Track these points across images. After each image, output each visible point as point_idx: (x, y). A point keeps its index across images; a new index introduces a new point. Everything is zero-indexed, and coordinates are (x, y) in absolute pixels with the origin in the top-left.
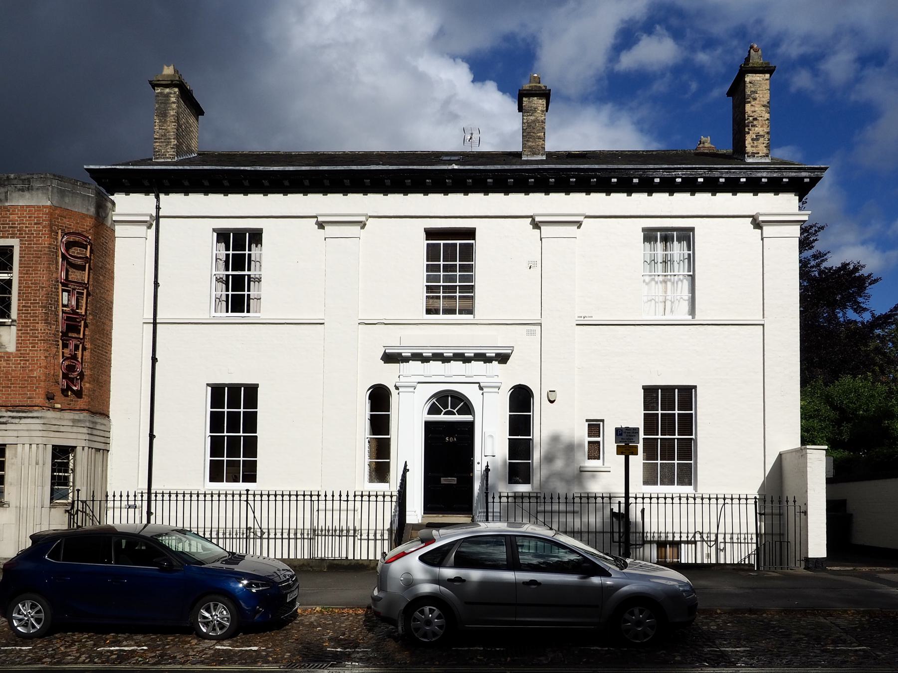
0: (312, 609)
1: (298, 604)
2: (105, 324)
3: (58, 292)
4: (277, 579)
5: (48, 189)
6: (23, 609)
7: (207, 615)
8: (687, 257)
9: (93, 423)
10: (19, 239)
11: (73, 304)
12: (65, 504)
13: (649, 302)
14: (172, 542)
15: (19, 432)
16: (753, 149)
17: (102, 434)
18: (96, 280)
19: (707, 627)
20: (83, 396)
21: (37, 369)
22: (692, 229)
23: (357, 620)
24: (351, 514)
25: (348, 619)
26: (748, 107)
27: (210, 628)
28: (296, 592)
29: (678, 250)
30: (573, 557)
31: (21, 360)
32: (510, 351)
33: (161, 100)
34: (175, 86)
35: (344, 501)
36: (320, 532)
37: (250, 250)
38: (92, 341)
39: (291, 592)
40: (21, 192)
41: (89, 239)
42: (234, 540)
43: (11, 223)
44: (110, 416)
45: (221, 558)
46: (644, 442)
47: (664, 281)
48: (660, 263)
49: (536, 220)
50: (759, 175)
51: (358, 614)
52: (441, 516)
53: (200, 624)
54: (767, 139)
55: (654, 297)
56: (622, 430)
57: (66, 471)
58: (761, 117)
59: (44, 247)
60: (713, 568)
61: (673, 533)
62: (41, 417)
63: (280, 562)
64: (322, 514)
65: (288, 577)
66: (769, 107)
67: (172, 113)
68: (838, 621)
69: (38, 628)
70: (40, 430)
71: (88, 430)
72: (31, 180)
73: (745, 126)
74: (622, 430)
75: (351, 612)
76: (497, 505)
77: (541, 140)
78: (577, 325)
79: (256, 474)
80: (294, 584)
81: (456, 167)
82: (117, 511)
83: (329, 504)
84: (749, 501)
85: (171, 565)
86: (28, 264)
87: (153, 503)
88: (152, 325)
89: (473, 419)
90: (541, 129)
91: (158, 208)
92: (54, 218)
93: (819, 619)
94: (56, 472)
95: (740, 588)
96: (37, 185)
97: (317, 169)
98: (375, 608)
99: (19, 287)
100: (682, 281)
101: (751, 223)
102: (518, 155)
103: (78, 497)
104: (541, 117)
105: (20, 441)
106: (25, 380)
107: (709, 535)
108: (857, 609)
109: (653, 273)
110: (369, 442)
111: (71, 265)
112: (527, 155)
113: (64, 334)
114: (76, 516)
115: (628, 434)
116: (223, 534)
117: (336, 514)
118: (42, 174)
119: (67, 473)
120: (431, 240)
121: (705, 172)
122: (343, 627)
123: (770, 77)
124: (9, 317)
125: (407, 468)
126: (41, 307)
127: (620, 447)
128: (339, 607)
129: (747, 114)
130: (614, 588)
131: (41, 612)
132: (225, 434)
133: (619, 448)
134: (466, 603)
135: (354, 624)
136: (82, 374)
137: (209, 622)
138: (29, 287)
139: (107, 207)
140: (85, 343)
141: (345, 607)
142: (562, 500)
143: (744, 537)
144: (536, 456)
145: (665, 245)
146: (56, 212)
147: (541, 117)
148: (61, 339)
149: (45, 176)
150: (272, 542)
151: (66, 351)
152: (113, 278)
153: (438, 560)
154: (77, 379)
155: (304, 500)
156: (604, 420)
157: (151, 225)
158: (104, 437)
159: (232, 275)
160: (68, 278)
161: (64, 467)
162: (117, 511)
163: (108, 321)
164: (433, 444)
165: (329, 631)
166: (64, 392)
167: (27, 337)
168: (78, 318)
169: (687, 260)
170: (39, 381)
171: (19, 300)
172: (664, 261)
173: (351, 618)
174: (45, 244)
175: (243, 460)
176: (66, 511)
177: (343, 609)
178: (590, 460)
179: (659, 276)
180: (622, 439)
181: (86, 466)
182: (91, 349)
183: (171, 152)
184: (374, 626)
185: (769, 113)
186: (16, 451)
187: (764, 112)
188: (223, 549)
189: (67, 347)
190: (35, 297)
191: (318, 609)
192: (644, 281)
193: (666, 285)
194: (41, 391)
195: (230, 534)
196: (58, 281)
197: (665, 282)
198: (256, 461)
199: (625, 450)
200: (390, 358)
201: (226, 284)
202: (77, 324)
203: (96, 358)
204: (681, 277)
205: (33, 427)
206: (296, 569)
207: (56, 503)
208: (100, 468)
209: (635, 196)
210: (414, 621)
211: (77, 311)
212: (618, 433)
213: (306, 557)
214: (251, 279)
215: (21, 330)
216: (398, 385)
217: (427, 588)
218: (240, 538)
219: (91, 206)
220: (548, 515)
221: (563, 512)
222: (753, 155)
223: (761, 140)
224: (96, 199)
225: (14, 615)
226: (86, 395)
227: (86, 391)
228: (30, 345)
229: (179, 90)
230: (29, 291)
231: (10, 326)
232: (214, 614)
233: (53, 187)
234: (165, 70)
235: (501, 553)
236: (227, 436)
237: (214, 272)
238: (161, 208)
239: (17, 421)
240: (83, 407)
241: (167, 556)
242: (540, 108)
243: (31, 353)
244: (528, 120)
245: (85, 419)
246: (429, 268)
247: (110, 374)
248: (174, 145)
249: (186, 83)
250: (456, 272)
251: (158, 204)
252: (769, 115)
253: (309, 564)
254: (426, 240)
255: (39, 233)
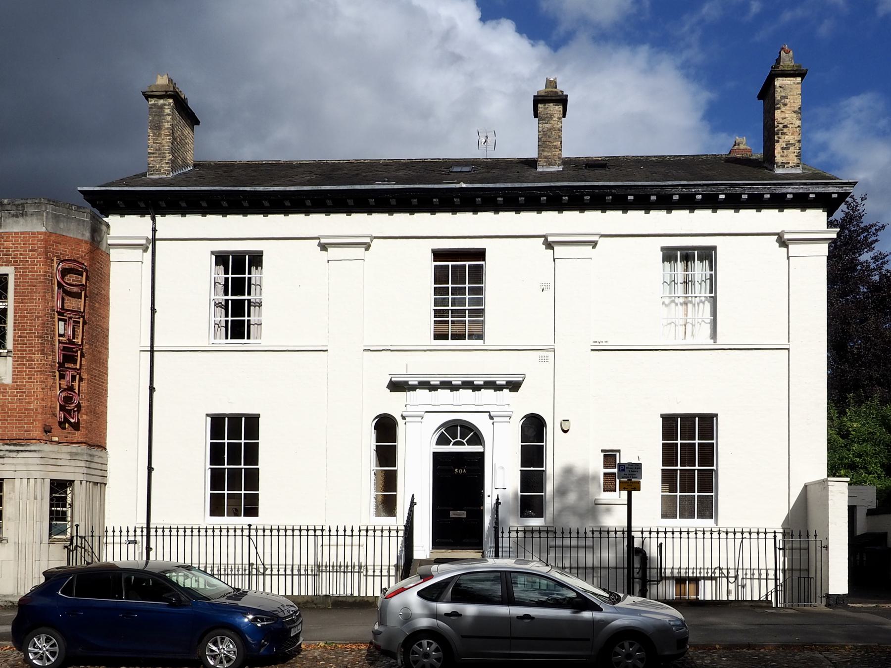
0: (315, 645)
1: (301, 639)
2: (101, 352)
3: (54, 321)
4: (281, 615)
5: (42, 215)
6: (38, 643)
7: (214, 648)
8: (709, 277)
9: (91, 455)
10: (13, 267)
11: (69, 333)
12: (64, 540)
13: (669, 326)
14: (180, 578)
15: (17, 466)
16: (783, 158)
17: (99, 467)
18: (92, 308)
19: (701, 661)
20: (80, 429)
21: (34, 401)
22: (714, 248)
23: (360, 655)
24: (356, 549)
25: (351, 654)
26: (778, 114)
27: (217, 660)
28: (299, 627)
29: (699, 269)
30: (574, 595)
31: (17, 392)
32: (521, 379)
33: (153, 112)
34: (170, 97)
35: (349, 536)
36: (324, 568)
37: (250, 273)
38: (89, 371)
39: (295, 627)
40: (15, 218)
41: (85, 265)
42: (230, 576)
43: (5, 250)
44: (107, 448)
45: (227, 594)
46: (662, 473)
47: (685, 304)
48: (681, 283)
49: (549, 240)
50: (784, 191)
51: (361, 649)
52: (450, 551)
53: (208, 657)
54: (798, 148)
55: (674, 321)
56: (624, 466)
57: (64, 506)
58: (792, 124)
59: (39, 275)
60: (730, 605)
61: (728, 569)
62: (39, 451)
63: (284, 598)
64: (326, 549)
65: (291, 613)
66: (800, 113)
67: (167, 125)
68: (833, 656)
69: (53, 661)
70: (38, 464)
71: (86, 463)
72: (25, 205)
73: (774, 134)
74: (624, 466)
75: (354, 647)
76: (506, 540)
77: (558, 150)
78: (592, 350)
79: (258, 508)
80: (297, 619)
81: (464, 185)
82: (117, 547)
83: (334, 539)
84: (768, 535)
85: (179, 600)
86: (23, 292)
87: (152, 539)
88: (149, 353)
89: (483, 450)
90: (557, 137)
91: (154, 230)
92: (50, 245)
93: (815, 654)
94: (54, 507)
95: (748, 624)
96: (31, 210)
97: (319, 189)
98: (376, 642)
99: (15, 316)
100: (703, 303)
101: (776, 241)
102: (531, 163)
103: (77, 533)
104: (558, 124)
105: (18, 475)
106: (22, 413)
107: (695, 571)
108: (855, 644)
109: (673, 295)
110: (375, 474)
111: (67, 293)
112: (543, 166)
113: (61, 365)
114: (75, 552)
115: (630, 470)
116: (218, 571)
117: (341, 549)
118: (36, 199)
119: (65, 507)
120: (440, 261)
121: (726, 188)
122: (345, 661)
123: (802, 81)
124: (4, 348)
125: (415, 501)
126: (38, 337)
127: (623, 483)
128: (342, 642)
129: (776, 121)
130: (604, 623)
131: (56, 646)
132: (226, 466)
133: (621, 484)
134: (463, 637)
135: (356, 658)
136: (79, 406)
137: (216, 655)
138: (25, 317)
139: (102, 230)
140: (82, 374)
141: (348, 642)
142: (574, 535)
143: (692, 571)
144: (549, 488)
145: (685, 265)
146: (52, 238)
147: (558, 124)
148: (58, 370)
149: (40, 202)
150: (275, 578)
151: (63, 382)
152: (108, 304)
153: (435, 595)
154: (74, 411)
155: (308, 535)
156: (620, 450)
157: (148, 248)
158: (101, 470)
159: (231, 300)
160: (64, 306)
161: (61, 502)
162: (117, 547)
163: (103, 349)
164: (442, 476)
165: (331, 665)
166: (61, 424)
167: (23, 368)
168: (74, 348)
169: (708, 280)
170: (36, 413)
171: (15, 330)
172: (684, 282)
173: (353, 653)
174: (40, 272)
175: (244, 494)
176: (65, 547)
177: (346, 644)
178: (606, 493)
179: (679, 297)
180: (625, 474)
181: (84, 503)
182: (88, 380)
183: (166, 167)
184: (376, 660)
185: (800, 120)
186: (14, 486)
187: (795, 119)
188: (224, 583)
189: (64, 378)
190: (31, 326)
191: (322, 644)
192: (663, 303)
193: (687, 307)
194: (39, 424)
195: (225, 571)
196: (54, 310)
197: (686, 304)
198: (258, 494)
199: (628, 485)
200: (396, 386)
201: (225, 309)
202: (74, 354)
203: (93, 388)
204: (703, 299)
205: (30, 461)
206: (300, 606)
207: (55, 538)
208: (98, 502)
209: (653, 213)
210: (413, 654)
211: (74, 340)
212: (621, 469)
213: (310, 594)
214: (252, 304)
215: (17, 361)
216: (404, 414)
217: (424, 623)
218: (235, 575)
219: (86, 231)
220: (559, 550)
221: (574, 547)
222: (783, 165)
223: (792, 149)
224: (91, 223)
225: (29, 649)
226: (83, 427)
227: (83, 423)
228: (27, 377)
229: (174, 100)
230: (25, 321)
231: (6, 356)
232: (221, 647)
233: (48, 213)
234: (158, 79)
235: (498, 589)
236: (228, 468)
237: (213, 297)
238: (157, 231)
239: (14, 454)
240: (80, 440)
241: (175, 592)
242: (557, 116)
243: (27, 384)
244: (543, 128)
245: (83, 452)
246: (437, 291)
247: (106, 404)
248: (169, 160)
249: (181, 91)
250: (466, 295)
251: (154, 226)
252: (800, 121)
253: (313, 601)
254: (434, 261)
255: (34, 261)
